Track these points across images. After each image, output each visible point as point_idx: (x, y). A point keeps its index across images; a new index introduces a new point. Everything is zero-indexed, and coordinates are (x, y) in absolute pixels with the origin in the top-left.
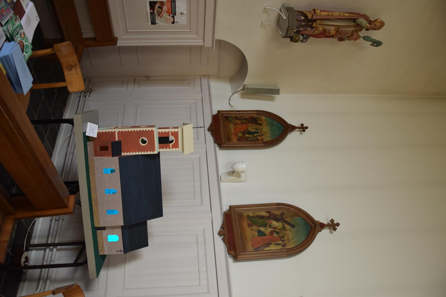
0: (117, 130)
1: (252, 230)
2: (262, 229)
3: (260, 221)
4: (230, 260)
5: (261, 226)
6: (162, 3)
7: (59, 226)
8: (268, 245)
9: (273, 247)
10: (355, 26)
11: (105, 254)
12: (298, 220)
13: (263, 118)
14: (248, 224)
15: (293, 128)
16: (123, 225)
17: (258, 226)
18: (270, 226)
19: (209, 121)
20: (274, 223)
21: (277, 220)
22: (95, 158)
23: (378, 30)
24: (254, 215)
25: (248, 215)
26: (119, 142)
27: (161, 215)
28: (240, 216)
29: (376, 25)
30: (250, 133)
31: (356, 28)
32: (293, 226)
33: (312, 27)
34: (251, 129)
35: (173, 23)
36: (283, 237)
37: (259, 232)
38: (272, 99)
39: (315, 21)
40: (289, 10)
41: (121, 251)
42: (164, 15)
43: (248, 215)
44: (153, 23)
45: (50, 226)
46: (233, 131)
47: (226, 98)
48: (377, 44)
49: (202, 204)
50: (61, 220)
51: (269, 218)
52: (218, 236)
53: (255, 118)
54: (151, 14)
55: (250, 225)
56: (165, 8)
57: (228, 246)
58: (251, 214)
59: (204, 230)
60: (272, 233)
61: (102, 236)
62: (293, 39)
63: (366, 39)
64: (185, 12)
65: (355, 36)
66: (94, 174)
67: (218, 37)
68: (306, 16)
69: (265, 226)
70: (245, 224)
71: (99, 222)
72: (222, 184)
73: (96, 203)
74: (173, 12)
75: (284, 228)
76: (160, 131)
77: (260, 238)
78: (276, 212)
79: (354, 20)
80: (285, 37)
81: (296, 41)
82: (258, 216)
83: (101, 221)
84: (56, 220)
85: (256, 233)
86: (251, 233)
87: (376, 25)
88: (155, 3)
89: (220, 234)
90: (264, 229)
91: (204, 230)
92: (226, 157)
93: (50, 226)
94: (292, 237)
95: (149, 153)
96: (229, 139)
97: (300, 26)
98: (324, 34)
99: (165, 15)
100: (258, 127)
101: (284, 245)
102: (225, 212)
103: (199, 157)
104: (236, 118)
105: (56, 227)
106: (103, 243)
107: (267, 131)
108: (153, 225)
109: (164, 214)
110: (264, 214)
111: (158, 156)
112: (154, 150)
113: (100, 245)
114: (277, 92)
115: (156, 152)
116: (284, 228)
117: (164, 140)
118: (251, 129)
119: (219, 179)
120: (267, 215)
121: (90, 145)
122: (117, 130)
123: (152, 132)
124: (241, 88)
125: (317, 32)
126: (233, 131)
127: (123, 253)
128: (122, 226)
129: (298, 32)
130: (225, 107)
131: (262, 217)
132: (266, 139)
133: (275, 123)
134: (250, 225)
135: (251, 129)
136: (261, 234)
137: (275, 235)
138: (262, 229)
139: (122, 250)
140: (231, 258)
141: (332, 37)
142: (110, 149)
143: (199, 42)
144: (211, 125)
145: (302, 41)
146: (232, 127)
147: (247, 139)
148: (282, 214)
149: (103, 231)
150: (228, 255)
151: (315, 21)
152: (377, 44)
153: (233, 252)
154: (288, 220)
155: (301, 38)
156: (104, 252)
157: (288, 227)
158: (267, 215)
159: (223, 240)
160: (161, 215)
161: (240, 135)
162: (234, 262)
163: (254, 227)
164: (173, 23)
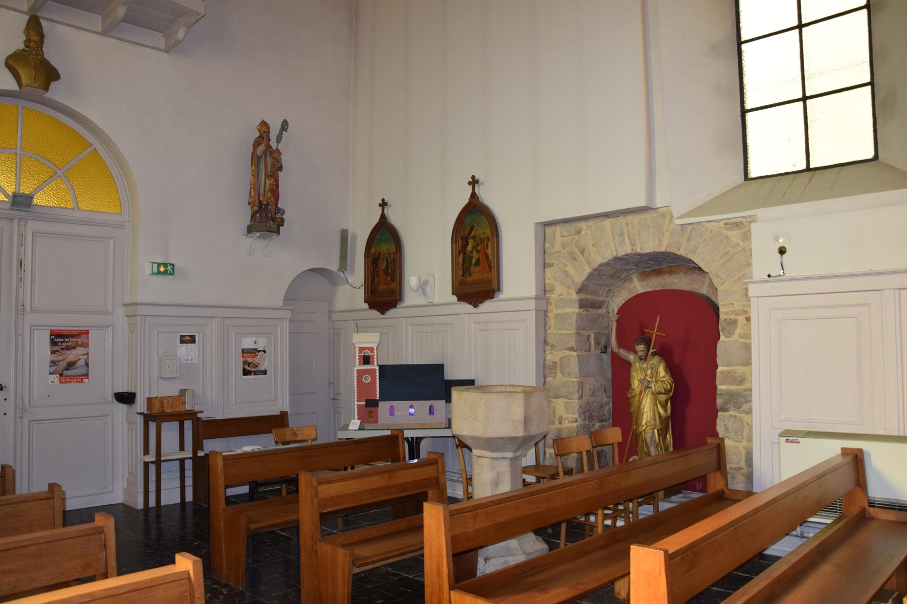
0: (356, 403)
2: (474, 261)
4: (501, 296)
5: (471, 262)
6: (245, 363)
8: (487, 256)
9: (489, 252)
10: (266, 156)
12: (467, 221)
13: (373, 250)
15: (383, 217)
18: (471, 252)
19: (466, 307)
20: (469, 248)
21: (467, 244)
22: (380, 423)
23: (269, 127)
26: (367, 401)
27: (442, 365)
28: (462, 284)
29: (264, 127)
30: (387, 268)
31: (268, 154)
32: (473, 227)
33: (268, 204)
34: (384, 266)
35: (265, 352)
36: (481, 239)
38: (355, 237)
39: (260, 202)
40: (250, 230)
42: (484, 461)
44: (265, 372)
46: (384, 287)
47: (352, 291)
48: (285, 126)
49: (525, 321)
51: (465, 253)
53: (373, 260)
54: (255, 374)
55: (470, 275)
56: (250, 360)
58: (461, 272)
60: (477, 252)
62: (282, 223)
63: (279, 139)
64: (254, 339)
65: (276, 156)
66: (394, 425)
67: (280, 303)
68: (257, 212)
69: (471, 258)
70: (469, 279)
72: (436, 301)
73: (423, 424)
74: (254, 352)
75: (474, 238)
76: (357, 363)
77: (481, 264)
78: (460, 245)
79: (259, 158)
80: (278, 232)
81: (283, 221)
82: (463, 265)
83: (440, 421)
86: (477, 274)
87: (264, 127)
88: (244, 370)
89: (476, 306)
92: (411, 297)
94: (482, 230)
95: (377, 374)
96: (393, 291)
97: (266, 217)
98: (275, 191)
99: (256, 360)
100: (381, 258)
101: (488, 238)
103: (475, 323)
104: (373, 282)
107: (386, 248)
110: (461, 258)
111: (382, 368)
112: (375, 370)
114: (344, 234)
115: (377, 368)
116: (474, 238)
117: (366, 360)
118: (383, 265)
119: (431, 305)
120: (462, 255)
121: (367, 426)
122: (356, 403)
123: (358, 370)
124: (341, 274)
125: (273, 199)
126: (384, 287)
129: (274, 219)
130: (361, 294)
131: (464, 261)
132: (393, 249)
133: (378, 237)
134: (470, 275)
135: (383, 265)
136: (477, 264)
137: (479, 248)
141: (277, 181)
142: (372, 409)
143: (286, 324)
145: (283, 214)
146: (382, 287)
147: (393, 271)
148: (462, 238)
151: (260, 202)
152: (285, 126)
154: (467, 231)
155: (279, 215)
157: (473, 233)
158: (462, 255)
160: (442, 365)
161: (389, 278)
163: (472, 270)
164: (265, 352)
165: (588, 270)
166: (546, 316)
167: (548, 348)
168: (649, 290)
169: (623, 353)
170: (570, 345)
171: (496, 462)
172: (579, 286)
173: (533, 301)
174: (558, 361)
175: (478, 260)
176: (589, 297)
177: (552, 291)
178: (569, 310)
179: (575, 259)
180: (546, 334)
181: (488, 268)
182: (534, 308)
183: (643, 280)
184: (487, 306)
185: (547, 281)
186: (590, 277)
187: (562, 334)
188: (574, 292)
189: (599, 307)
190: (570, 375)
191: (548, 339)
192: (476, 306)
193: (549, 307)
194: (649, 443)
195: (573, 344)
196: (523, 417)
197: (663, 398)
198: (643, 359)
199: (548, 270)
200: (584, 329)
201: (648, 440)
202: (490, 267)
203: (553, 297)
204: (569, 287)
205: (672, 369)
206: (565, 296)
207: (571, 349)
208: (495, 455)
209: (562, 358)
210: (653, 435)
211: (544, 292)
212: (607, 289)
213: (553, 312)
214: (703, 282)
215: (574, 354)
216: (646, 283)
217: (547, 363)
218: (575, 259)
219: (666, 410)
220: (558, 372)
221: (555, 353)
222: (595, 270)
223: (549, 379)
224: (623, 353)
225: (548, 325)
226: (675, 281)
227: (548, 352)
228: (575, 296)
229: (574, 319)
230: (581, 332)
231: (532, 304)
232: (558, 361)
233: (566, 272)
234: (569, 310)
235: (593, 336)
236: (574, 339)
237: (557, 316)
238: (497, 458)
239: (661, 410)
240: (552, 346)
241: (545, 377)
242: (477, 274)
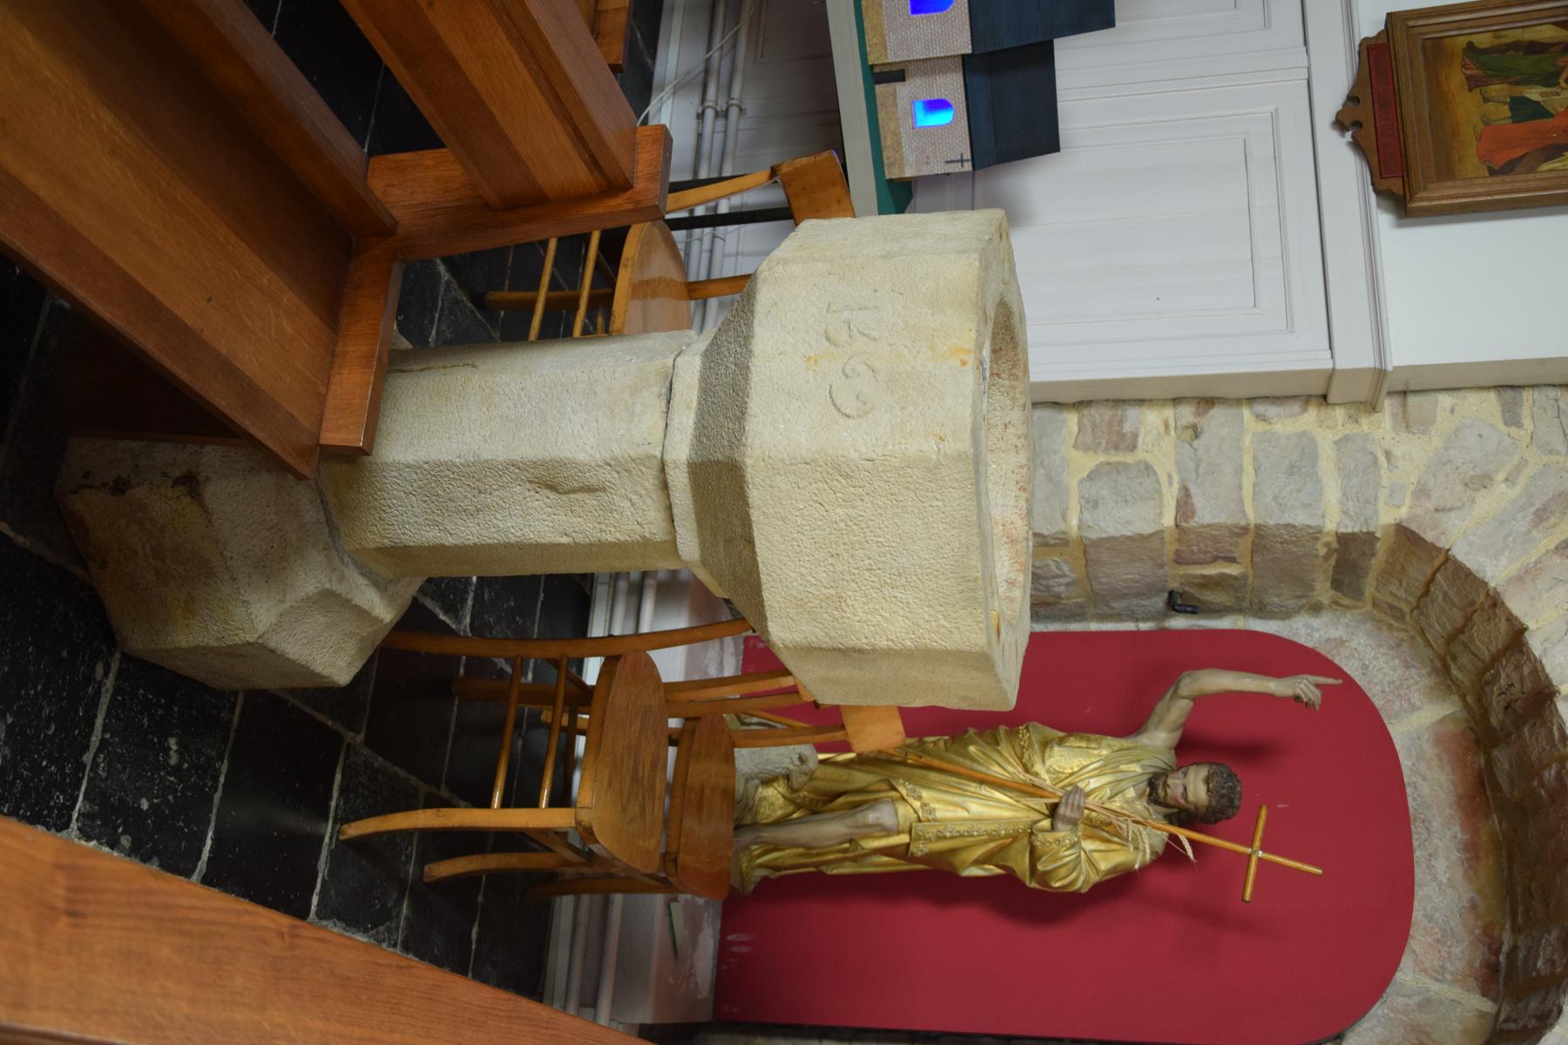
1: (1486, 100)
2: (1534, 93)
3: (1526, 63)
4: (1384, 220)
5: (1529, 81)
7: (730, 144)
11: (909, 173)
14: (1469, 78)
16: (969, 51)
17: (1518, 83)
19: (1336, 78)
24: (1497, 42)
25: (1470, 44)
28: (1435, 51)
37: (1523, 110)
41: (962, 161)
42: (651, 420)
43: (1470, 44)
45: (700, 136)
50: (734, 112)
52: (1335, 134)
55: (1473, 83)
57: (1375, 159)
58: (1483, 40)
59: (1274, 117)
61: (895, 105)
70: (1455, 79)
71: (885, 47)
77: (1524, 128)
82: (1516, 46)
83: (891, 40)
84: (717, 114)
85: (1505, 111)
89: (1340, 124)
90: (1542, 94)
91: (1274, 117)
93: (700, 136)
102: (1366, 39)
105: (718, 138)
106: (897, 134)
108: (1076, 60)
109: (1118, 14)
113: (889, 142)
127: (968, 167)
128: (963, 56)
131: (1534, 48)
134: (1473, 83)
136: (1523, 110)
138: (1534, 93)
139: (968, 155)
140: (1388, 211)
144: (1352, 98)
149: (898, 86)
150: (1373, 196)
153: (1396, 185)
156: (902, 167)
159: (1356, 145)
160: (1108, 21)
162: (1400, 226)
163: (1497, 90)
165: (1494, 571)
166: (1306, 400)
167: (1187, 413)
168: (1405, 763)
169: (1174, 712)
170: (1199, 502)
171: (650, 481)
172: (1429, 536)
173: (1367, 361)
174: (1140, 455)
175: (1539, 111)
176: (1377, 563)
177: (1406, 422)
178: (1332, 495)
179: (1541, 516)
180: (1238, 402)
181: (1501, 159)
182: (1344, 362)
183: (1439, 740)
184: (1345, 168)
185: (1446, 400)
186: (1463, 576)
187: (1239, 470)
188: (1402, 513)
189: (1337, 584)
190: (1092, 503)
191: (1218, 414)
192: (1340, 124)
193: (1340, 413)
194: (860, 818)
195: (1207, 514)
196: (863, 643)
197: (1021, 865)
198: (1154, 788)
199: (1486, 405)
200: (1256, 549)
201: (872, 817)
202: (1508, 168)
203: (1382, 426)
204: (1422, 492)
205: (1119, 885)
206: (1386, 478)
207: (1185, 505)
208: (680, 481)
209: (1148, 469)
210: (888, 832)
211: (1394, 390)
212: (1406, 609)
213: (1323, 429)
214: (1439, 975)
215: (1168, 520)
216: (1430, 750)
217: (1132, 413)
218: (1541, 516)
219: (979, 862)
220: (1102, 458)
221: (1169, 443)
222: (1495, 602)
223: (1072, 419)
224: (1174, 712)
225: (1271, 410)
226: (1441, 865)
227: (1169, 412)
228: (1386, 516)
229: (1300, 518)
230: (1249, 539)
231: (1355, 355)
232: (1140, 455)
233: (1482, 481)
234: (1332, 495)
235: (1233, 570)
236: (1223, 518)
237: (1307, 447)
238: (665, 486)
239: (978, 852)
240: (1196, 432)
241: (1079, 405)
242: (1476, 111)
